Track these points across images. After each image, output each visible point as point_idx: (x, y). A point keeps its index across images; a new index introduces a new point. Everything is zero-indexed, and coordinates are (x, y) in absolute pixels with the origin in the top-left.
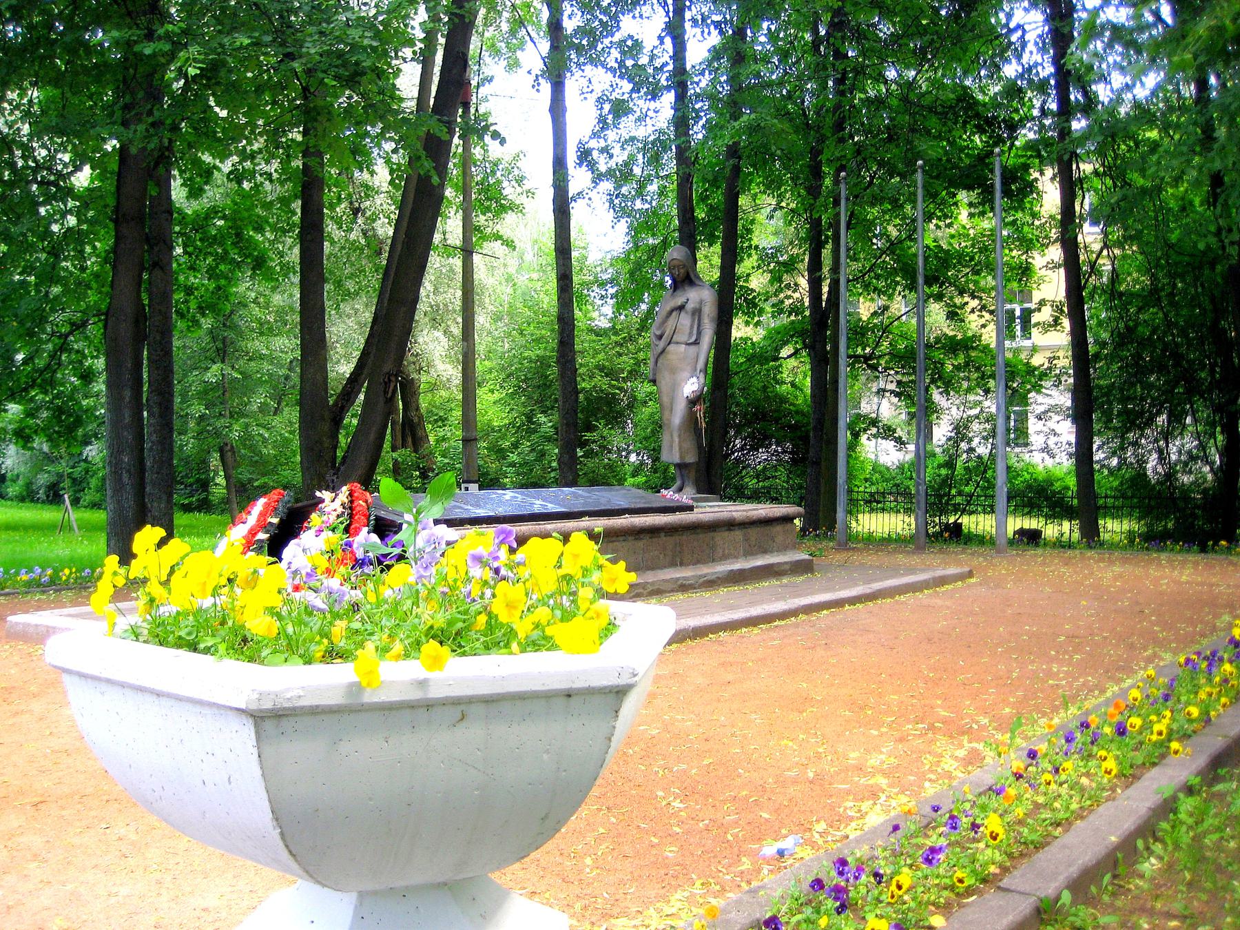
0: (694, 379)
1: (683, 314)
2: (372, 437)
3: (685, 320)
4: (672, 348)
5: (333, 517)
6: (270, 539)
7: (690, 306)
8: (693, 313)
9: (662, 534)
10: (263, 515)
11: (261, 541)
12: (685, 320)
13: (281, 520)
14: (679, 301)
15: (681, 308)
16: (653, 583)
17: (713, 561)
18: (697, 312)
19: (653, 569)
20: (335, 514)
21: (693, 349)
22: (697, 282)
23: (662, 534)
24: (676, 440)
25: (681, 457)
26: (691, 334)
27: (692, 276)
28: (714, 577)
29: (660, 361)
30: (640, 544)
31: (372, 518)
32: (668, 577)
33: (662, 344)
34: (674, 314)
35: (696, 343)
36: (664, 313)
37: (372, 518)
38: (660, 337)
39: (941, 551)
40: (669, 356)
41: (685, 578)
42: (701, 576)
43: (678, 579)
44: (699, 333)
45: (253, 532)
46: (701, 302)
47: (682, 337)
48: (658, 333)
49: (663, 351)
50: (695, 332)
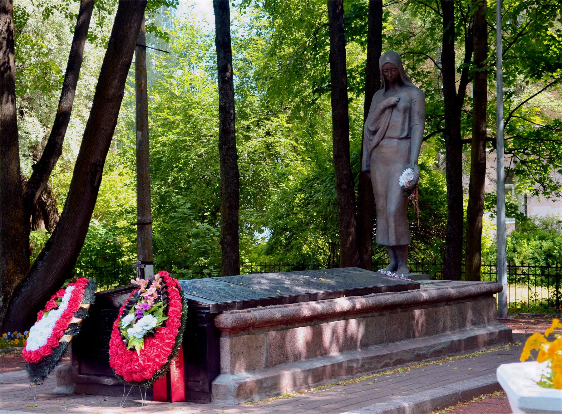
0: (409, 171)
1: (395, 112)
2: (78, 224)
3: (397, 118)
4: (385, 142)
5: (150, 302)
6: (82, 323)
7: (401, 105)
8: (405, 112)
9: (399, 310)
10: (74, 301)
11: (75, 324)
12: (397, 118)
13: (91, 305)
14: (392, 100)
15: (393, 107)
16: (396, 354)
17: (437, 333)
18: (408, 110)
19: (393, 341)
20: (152, 298)
21: (405, 144)
22: (407, 83)
23: (399, 310)
24: (392, 225)
25: (397, 240)
26: (403, 130)
27: (402, 78)
28: (439, 348)
29: (374, 154)
30: (384, 319)
31: (185, 301)
32: (407, 348)
33: (376, 138)
34: (387, 111)
35: (408, 137)
36: (378, 111)
37: (185, 301)
38: (374, 133)
39: (395, 302)
40: (384, 150)
41: (420, 349)
42: (431, 347)
43: (414, 350)
44: (410, 129)
45: (66, 316)
46: (411, 101)
47: (395, 132)
48: (372, 129)
49: (377, 145)
50: (406, 127)
